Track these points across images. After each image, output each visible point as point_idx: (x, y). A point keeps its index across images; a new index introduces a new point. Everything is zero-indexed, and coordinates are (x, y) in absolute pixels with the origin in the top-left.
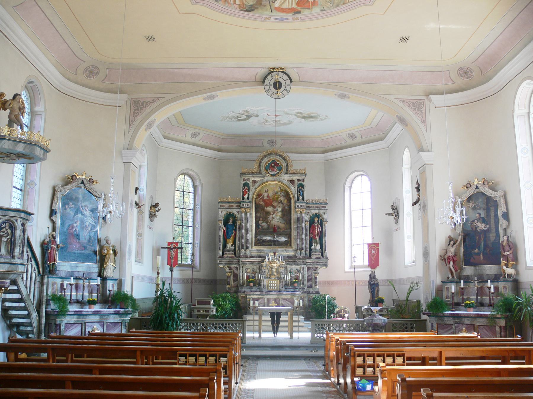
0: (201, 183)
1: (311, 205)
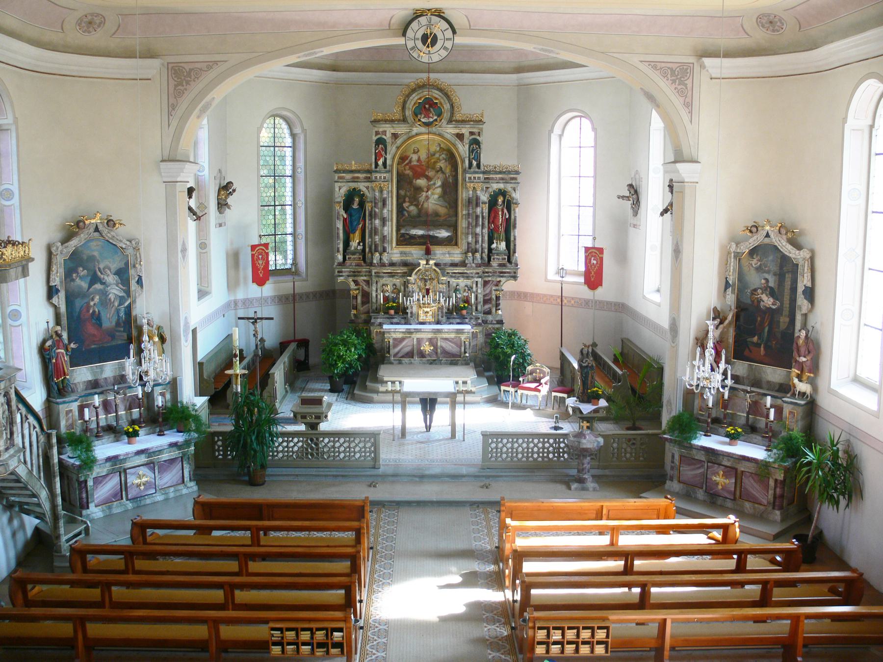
0: (304, 131)
1: (491, 176)
